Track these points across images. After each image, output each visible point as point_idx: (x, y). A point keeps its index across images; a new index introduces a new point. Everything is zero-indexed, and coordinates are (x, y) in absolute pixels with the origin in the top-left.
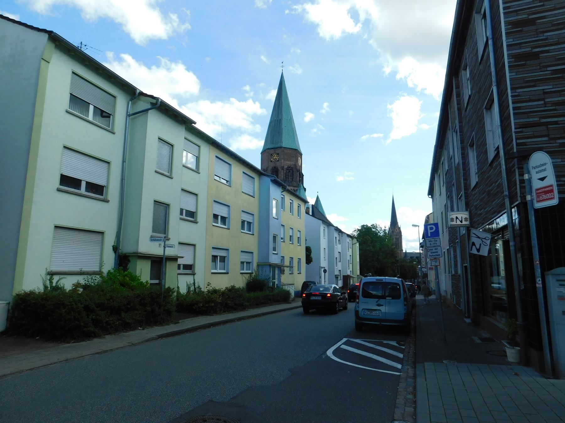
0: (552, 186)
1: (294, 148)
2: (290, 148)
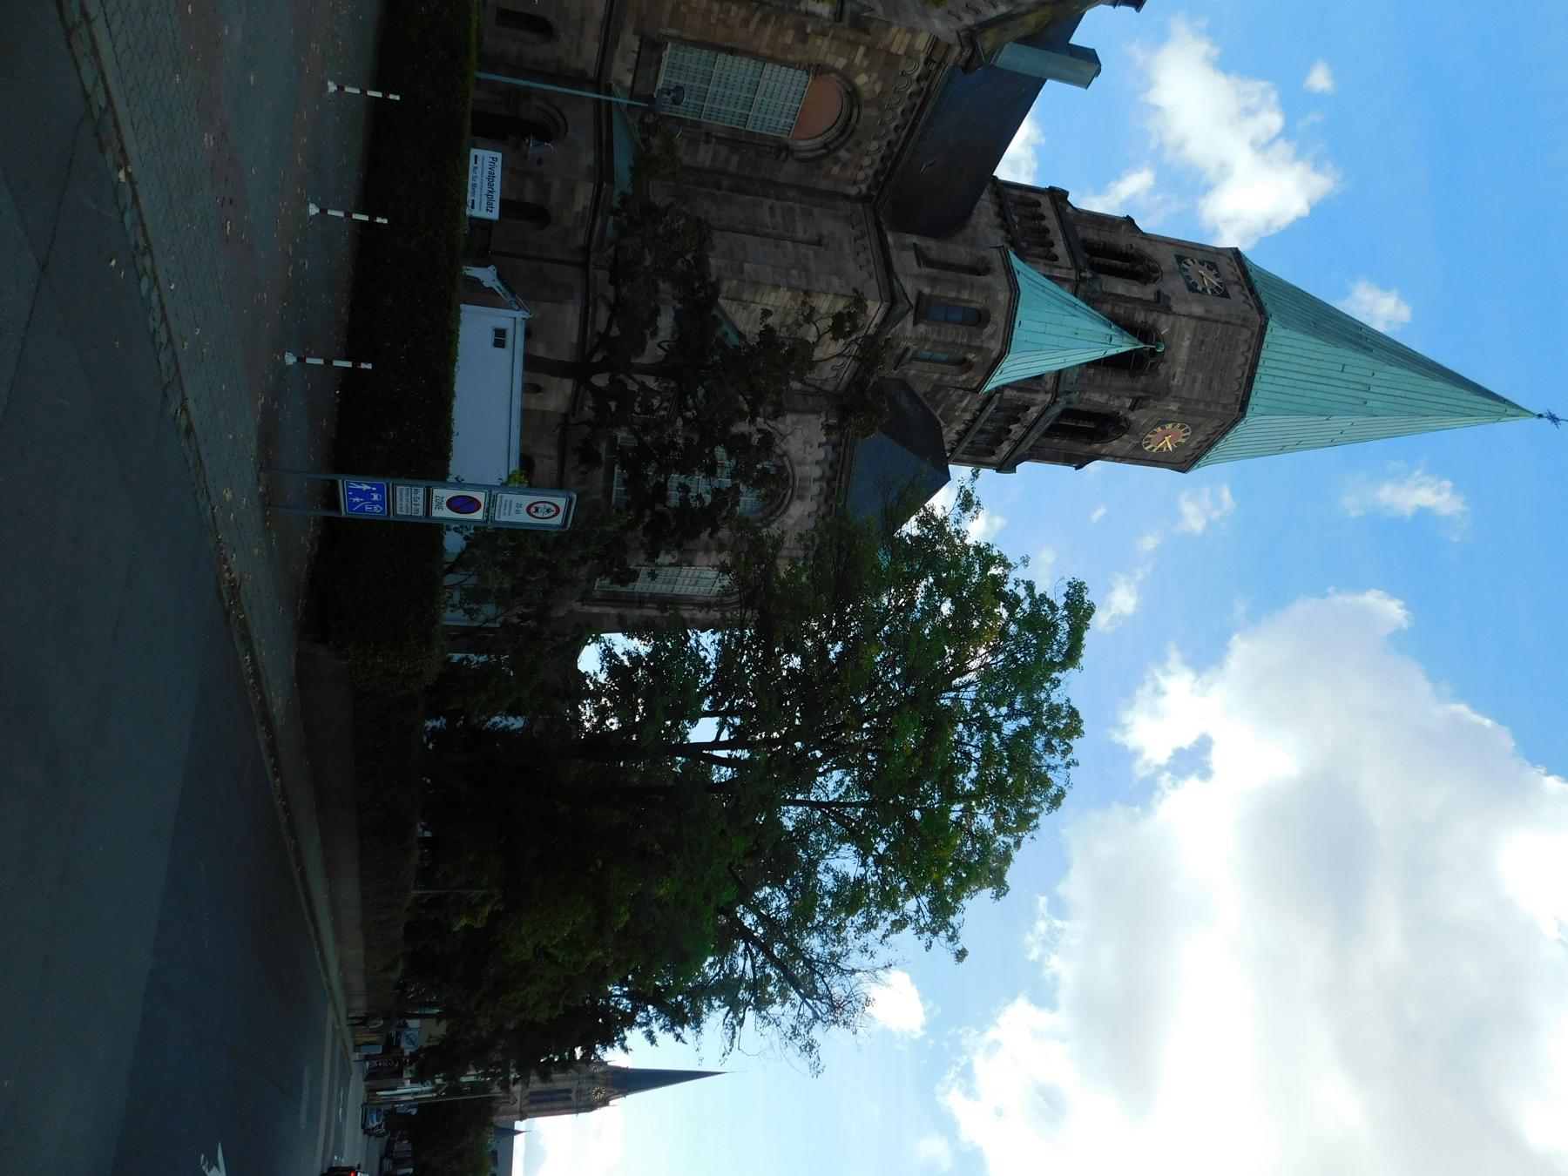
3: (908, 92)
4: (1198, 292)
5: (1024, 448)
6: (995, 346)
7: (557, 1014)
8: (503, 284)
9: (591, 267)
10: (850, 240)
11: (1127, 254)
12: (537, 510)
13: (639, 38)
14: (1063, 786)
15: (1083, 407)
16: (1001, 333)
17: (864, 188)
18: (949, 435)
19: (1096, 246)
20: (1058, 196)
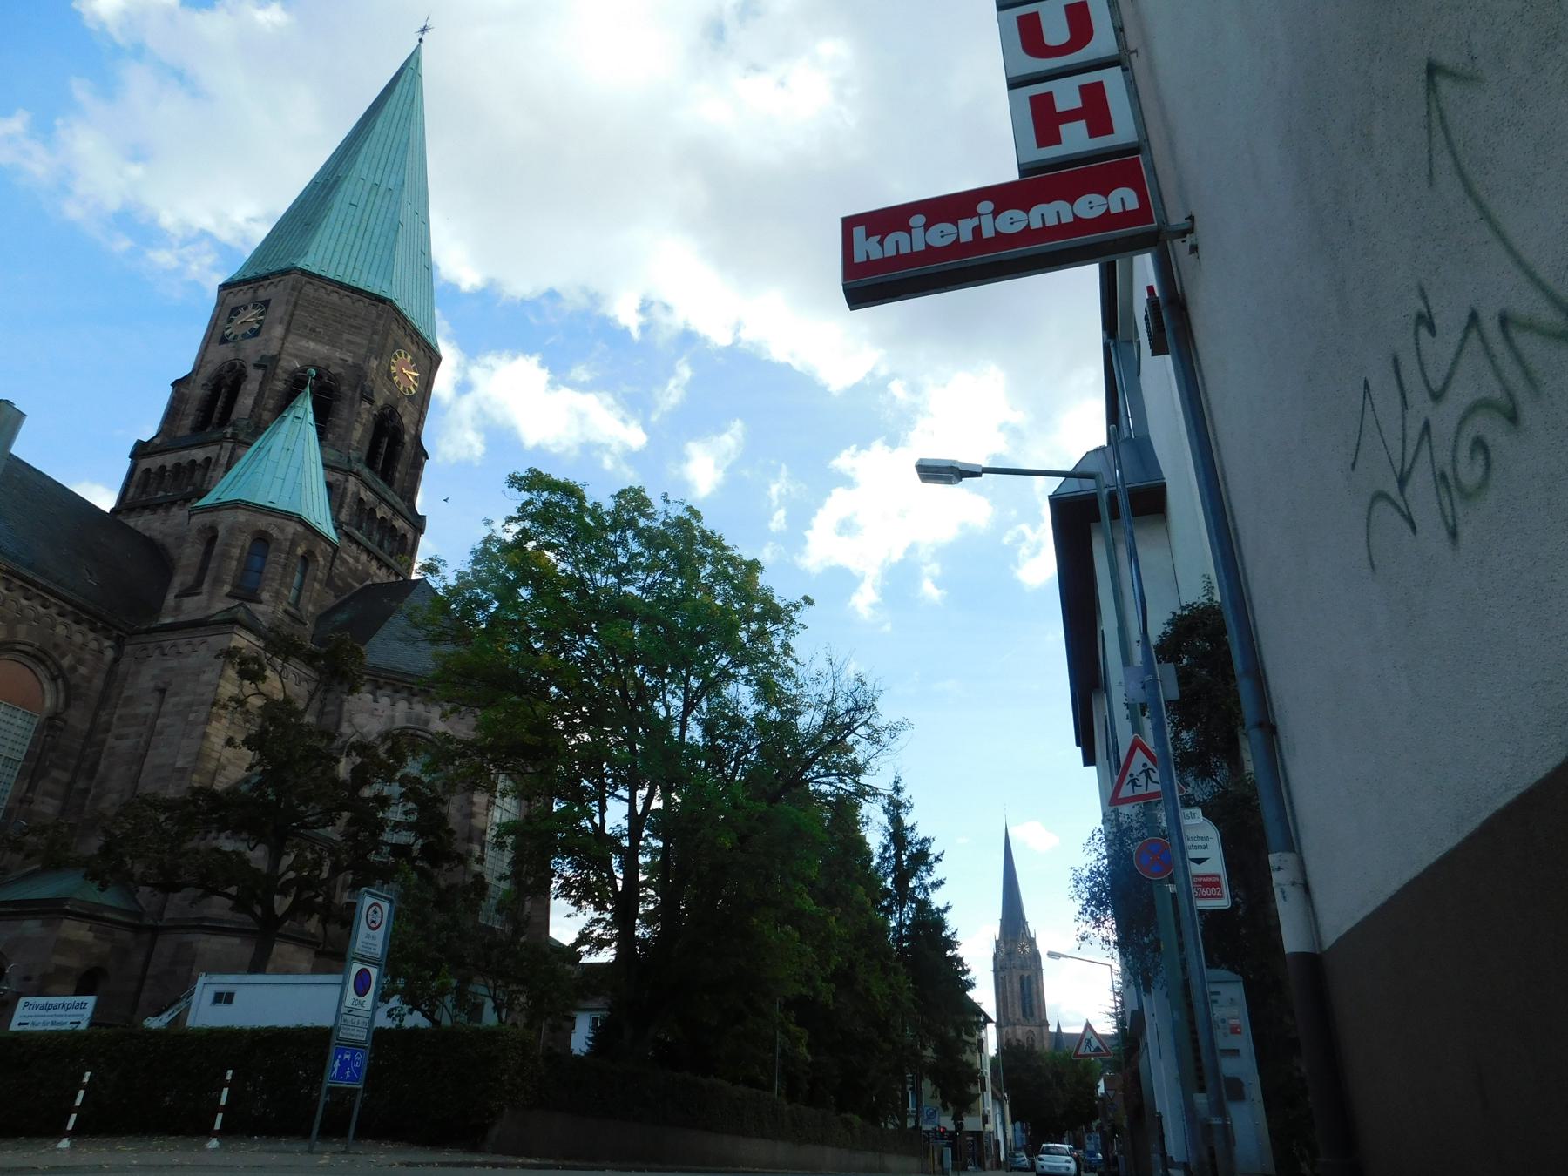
0: (1218, 876)
1: (369, 290)
2: (342, 286)
3: (5, 592)
4: (260, 328)
5: (402, 506)
6: (292, 527)
7: (902, 968)
8: (166, 1010)
9: (160, 924)
10: (163, 660)
12: (373, 922)
14: (684, 507)
15: (366, 448)
16: (279, 521)
17: (107, 643)
18: (381, 576)
19: (200, 419)
20: (141, 451)
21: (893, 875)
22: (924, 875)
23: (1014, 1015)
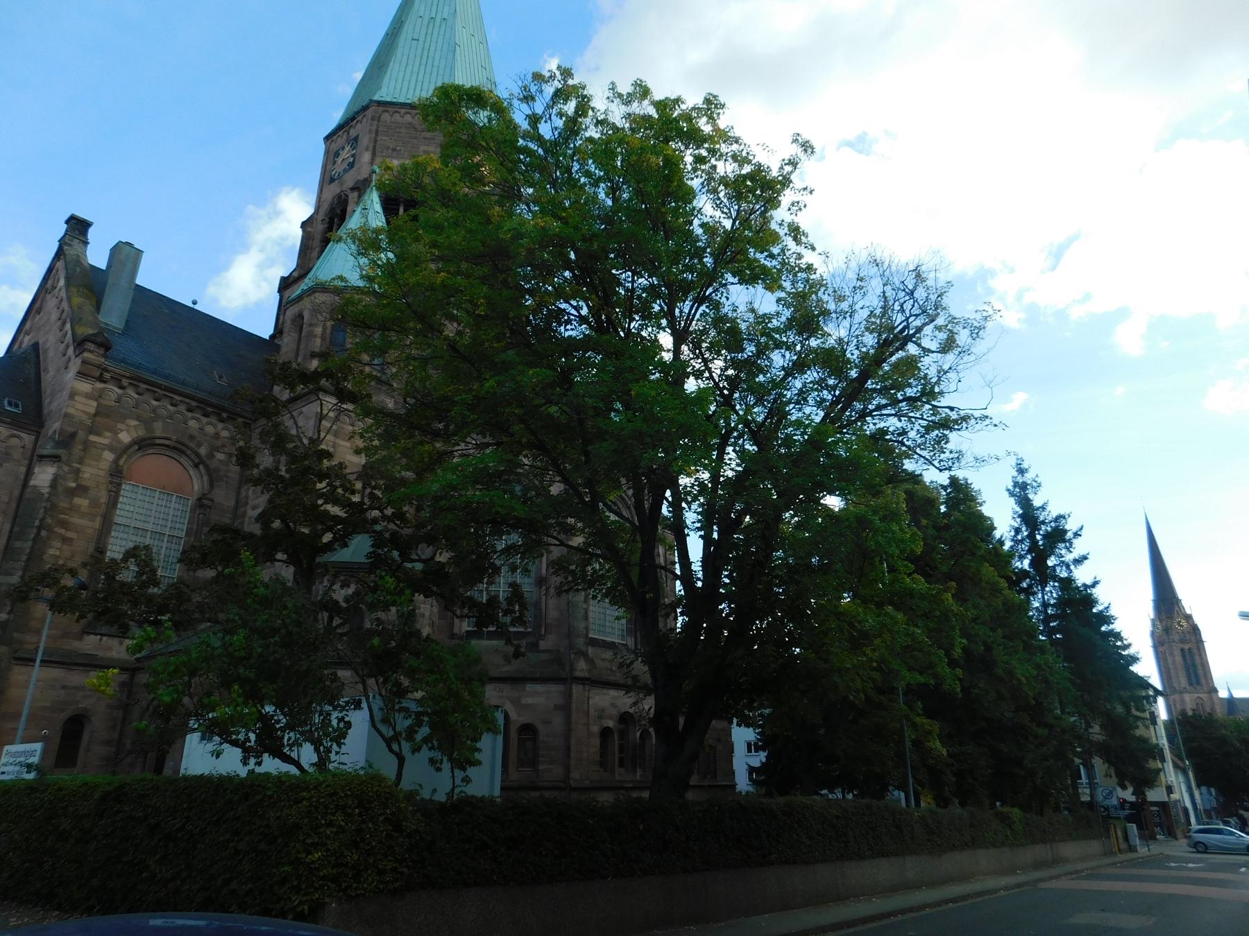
3: (136, 396)
4: (354, 160)
11: (329, 223)
13: (85, 635)
21: (1029, 557)
22: (1063, 552)
23: (1179, 683)
